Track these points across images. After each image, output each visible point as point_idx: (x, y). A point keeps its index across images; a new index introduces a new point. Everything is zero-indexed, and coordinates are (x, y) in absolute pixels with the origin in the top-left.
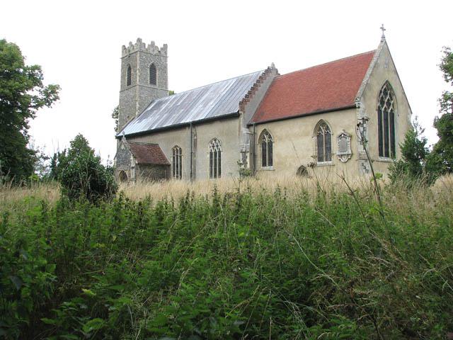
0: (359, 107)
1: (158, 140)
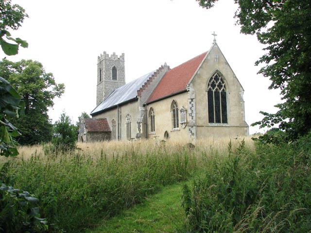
0: (189, 91)
1: (106, 116)
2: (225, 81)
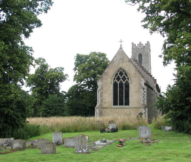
2: (128, 75)
